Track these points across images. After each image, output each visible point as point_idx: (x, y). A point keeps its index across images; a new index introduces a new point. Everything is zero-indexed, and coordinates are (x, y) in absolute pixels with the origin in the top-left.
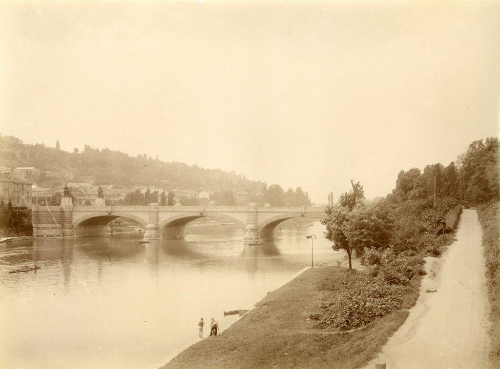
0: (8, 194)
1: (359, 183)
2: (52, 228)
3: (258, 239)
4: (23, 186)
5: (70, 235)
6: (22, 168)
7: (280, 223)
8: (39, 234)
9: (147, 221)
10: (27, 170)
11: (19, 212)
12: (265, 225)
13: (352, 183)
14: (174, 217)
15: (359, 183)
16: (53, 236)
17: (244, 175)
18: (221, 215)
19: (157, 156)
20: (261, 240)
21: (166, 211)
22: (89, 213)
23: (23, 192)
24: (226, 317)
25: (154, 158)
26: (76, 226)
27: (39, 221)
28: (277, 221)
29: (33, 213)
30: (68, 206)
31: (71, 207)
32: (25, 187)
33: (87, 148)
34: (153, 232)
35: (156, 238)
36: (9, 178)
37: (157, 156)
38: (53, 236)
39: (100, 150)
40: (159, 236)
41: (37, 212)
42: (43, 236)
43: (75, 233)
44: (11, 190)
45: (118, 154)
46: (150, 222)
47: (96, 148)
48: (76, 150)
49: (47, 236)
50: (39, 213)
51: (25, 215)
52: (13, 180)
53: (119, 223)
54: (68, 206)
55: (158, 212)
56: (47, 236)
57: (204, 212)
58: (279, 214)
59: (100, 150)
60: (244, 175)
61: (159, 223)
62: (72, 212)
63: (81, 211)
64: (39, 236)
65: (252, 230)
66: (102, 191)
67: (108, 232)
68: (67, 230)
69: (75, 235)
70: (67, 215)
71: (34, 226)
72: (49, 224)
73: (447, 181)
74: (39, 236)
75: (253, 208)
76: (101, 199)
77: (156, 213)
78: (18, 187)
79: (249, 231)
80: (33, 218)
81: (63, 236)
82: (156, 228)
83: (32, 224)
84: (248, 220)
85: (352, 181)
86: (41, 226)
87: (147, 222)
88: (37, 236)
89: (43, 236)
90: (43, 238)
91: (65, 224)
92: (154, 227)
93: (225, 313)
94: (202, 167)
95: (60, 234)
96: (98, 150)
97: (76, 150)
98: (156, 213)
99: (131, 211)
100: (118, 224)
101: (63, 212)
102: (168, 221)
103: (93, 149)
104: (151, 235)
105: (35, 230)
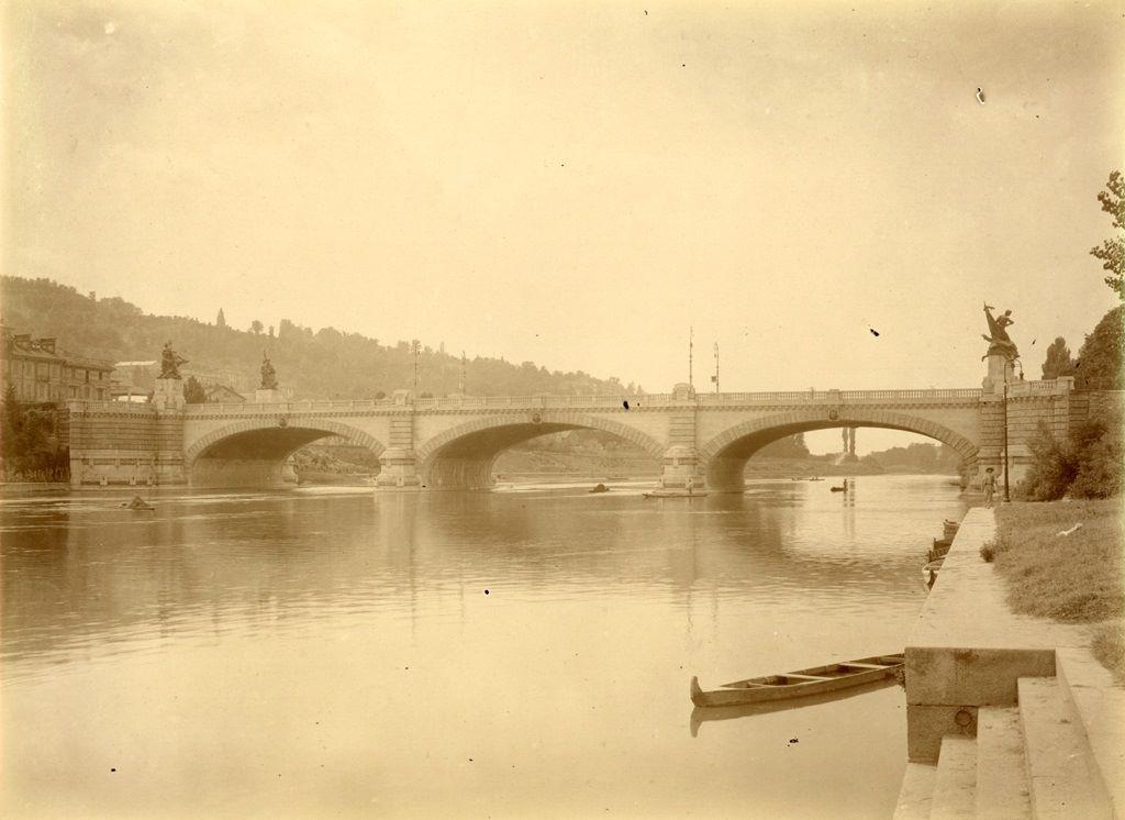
0: (46, 393)
1: (1008, 313)
2: (124, 462)
3: (701, 486)
4: (87, 372)
5: (176, 483)
6: (128, 363)
7: (779, 437)
8: (88, 478)
9: (385, 441)
10: (137, 367)
11: (32, 414)
12: (721, 445)
13: (989, 316)
14: (459, 427)
15: (1008, 313)
16: (127, 484)
17: (639, 387)
18: (593, 418)
19: (443, 343)
20: (708, 489)
21: (437, 413)
22: (225, 423)
23: (88, 389)
24: (708, 727)
25: (435, 349)
26: (191, 456)
27: (88, 443)
28: (769, 430)
29: (72, 419)
30: (170, 401)
31: (179, 406)
32: (94, 377)
33: (286, 325)
34: (401, 469)
35: (407, 489)
36: (53, 353)
37: (443, 343)
38: (127, 484)
39: (315, 332)
40: (417, 484)
41: (85, 415)
42: (98, 483)
43: (189, 477)
44: (55, 381)
45: (357, 339)
46: (392, 444)
47: (305, 325)
48: (257, 325)
49: (109, 483)
50: (148, 455)
51: (49, 425)
52: (61, 357)
53: (324, 463)
54: (170, 401)
55: (414, 414)
56: (109, 483)
57: (543, 410)
58: (762, 414)
59: (315, 332)
60: (639, 387)
61: (418, 446)
62: (183, 418)
63: (207, 418)
64: (88, 483)
65: (682, 461)
66: (273, 372)
67: (286, 481)
68: (167, 469)
69: (190, 484)
70: (168, 427)
71: (72, 454)
72: (116, 451)
73: (992, 470)
74: (88, 483)
75: (685, 398)
76: (270, 391)
77: (409, 419)
78: (74, 375)
79: (676, 462)
80: (74, 433)
81: (157, 484)
82: (410, 461)
83: (68, 448)
84: (672, 434)
85: (986, 308)
86: (92, 455)
87: (386, 444)
88: (83, 483)
89: (98, 483)
90: (97, 488)
91: (161, 453)
92: (403, 456)
93: (700, 698)
94: (543, 368)
95: (147, 477)
96: (309, 330)
97: (257, 325)
98: (409, 419)
99: (341, 415)
100: (319, 465)
101: (157, 417)
102: (443, 441)
103: (299, 329)
104: (394, 477)
105: (74, 466)
